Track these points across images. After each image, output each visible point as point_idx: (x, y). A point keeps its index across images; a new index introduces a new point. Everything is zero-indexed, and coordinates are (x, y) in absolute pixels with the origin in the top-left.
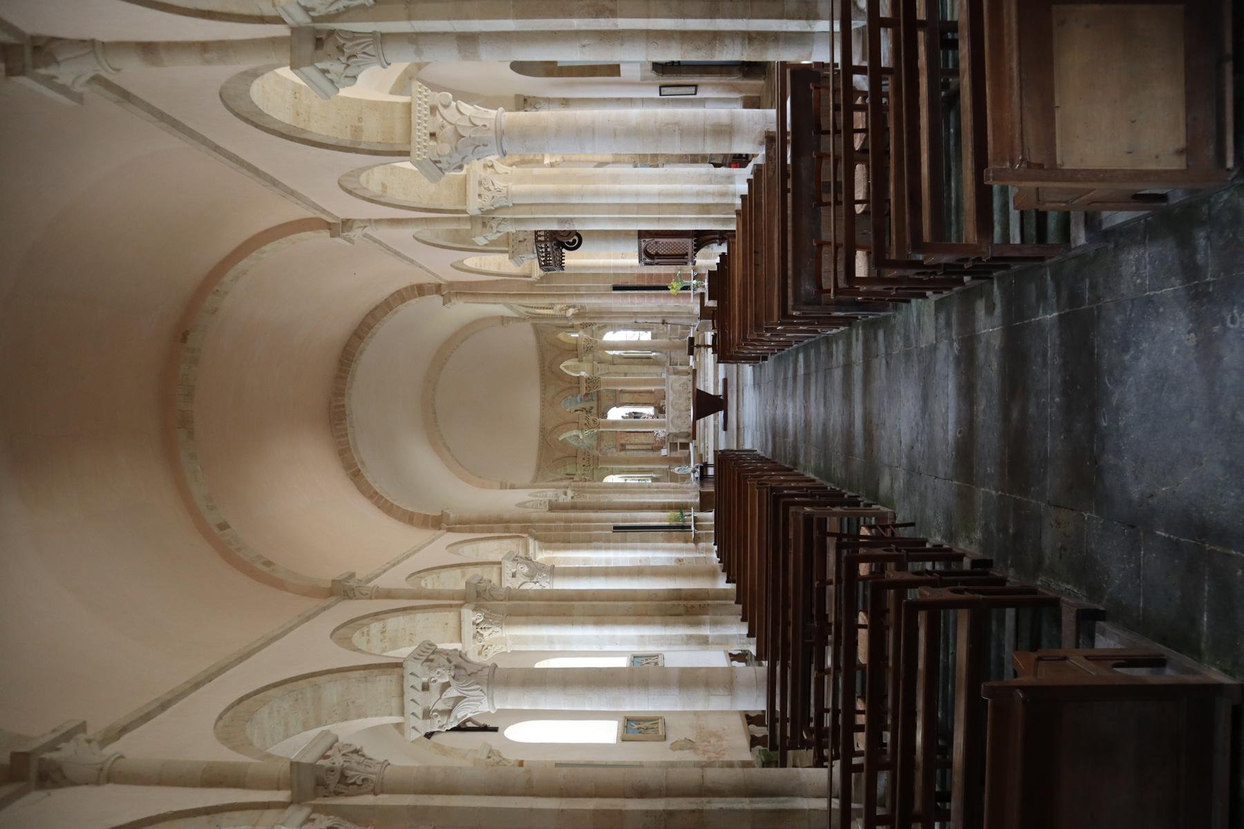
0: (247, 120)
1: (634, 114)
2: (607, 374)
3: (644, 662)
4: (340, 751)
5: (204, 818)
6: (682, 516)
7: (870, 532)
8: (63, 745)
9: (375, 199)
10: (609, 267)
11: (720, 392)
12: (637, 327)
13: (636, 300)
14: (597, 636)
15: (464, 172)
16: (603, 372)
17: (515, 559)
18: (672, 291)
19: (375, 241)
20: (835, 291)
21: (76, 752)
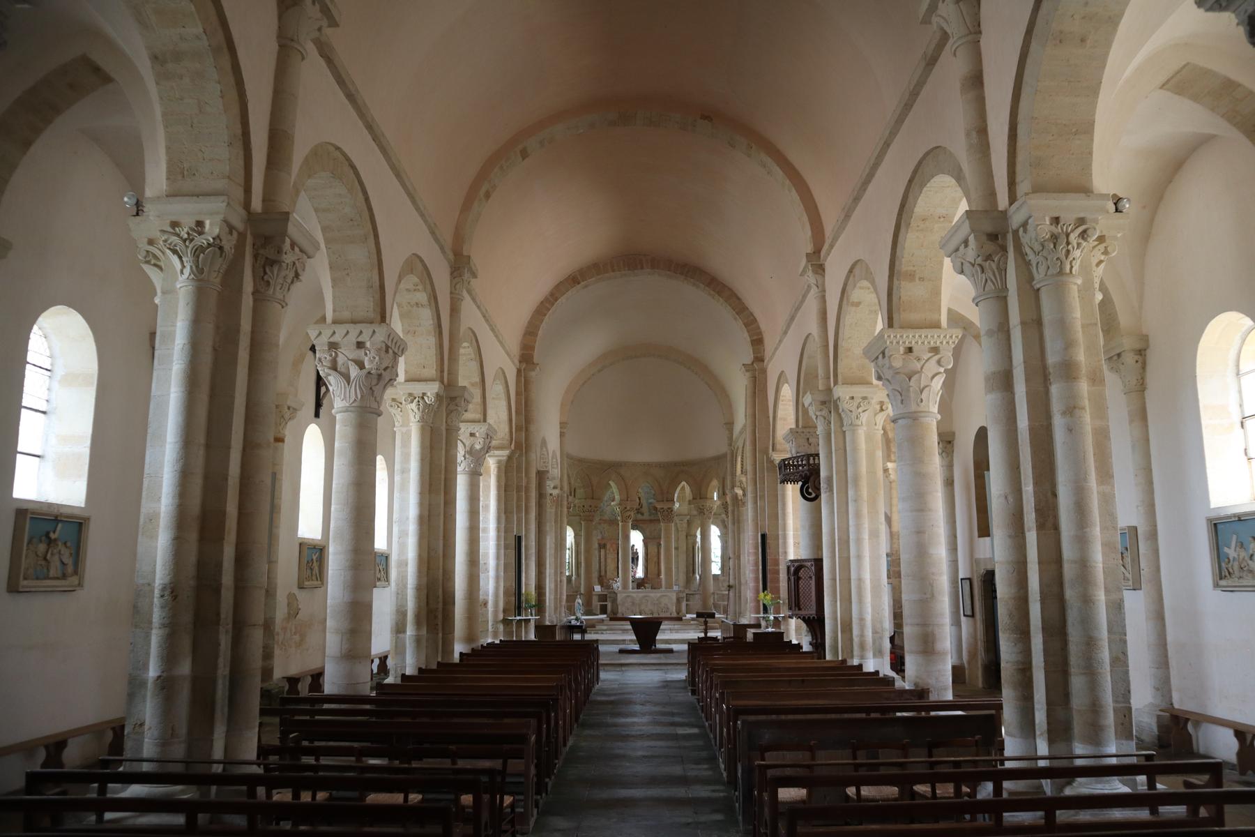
0: (915, 172)
1: (940, 552)
2: (677, 530)
3: (381, 567)
4: (298, 259)
5: (239, 132)
6: (531, 607)
7: (507, 807)
8: (317, 6)
9: (845, 295)
10: (785, 529)
11: (659, 646)
12: (724, 559)
13: (752, 558)
14: (408, 518)
15: (875, 382)
16: (679, 525)
17: (488, 437)
18: (762, 595)
19: (804, 297)
20: (763, 765)
21: (310, 18)
